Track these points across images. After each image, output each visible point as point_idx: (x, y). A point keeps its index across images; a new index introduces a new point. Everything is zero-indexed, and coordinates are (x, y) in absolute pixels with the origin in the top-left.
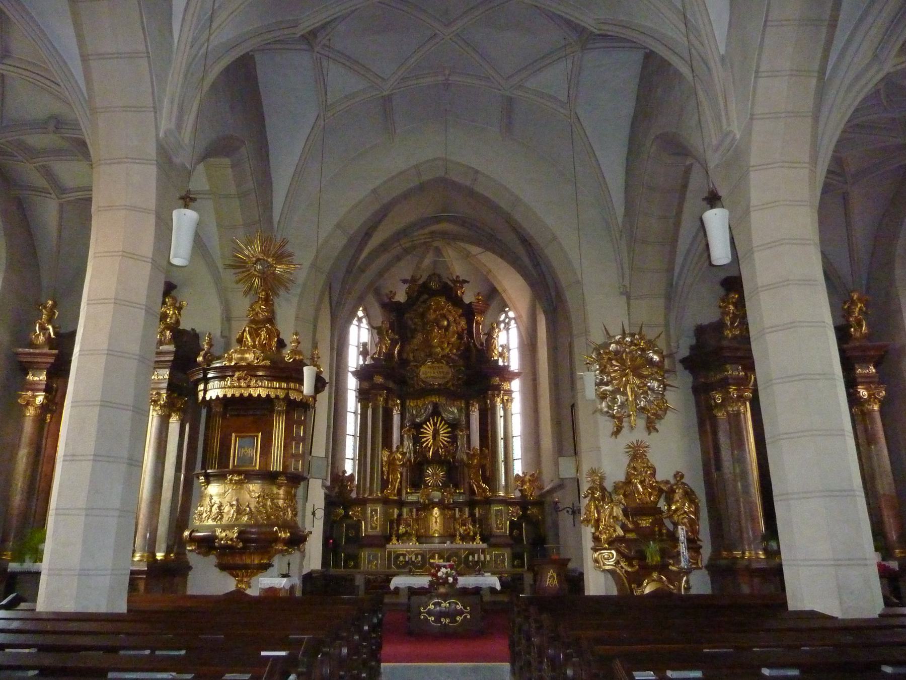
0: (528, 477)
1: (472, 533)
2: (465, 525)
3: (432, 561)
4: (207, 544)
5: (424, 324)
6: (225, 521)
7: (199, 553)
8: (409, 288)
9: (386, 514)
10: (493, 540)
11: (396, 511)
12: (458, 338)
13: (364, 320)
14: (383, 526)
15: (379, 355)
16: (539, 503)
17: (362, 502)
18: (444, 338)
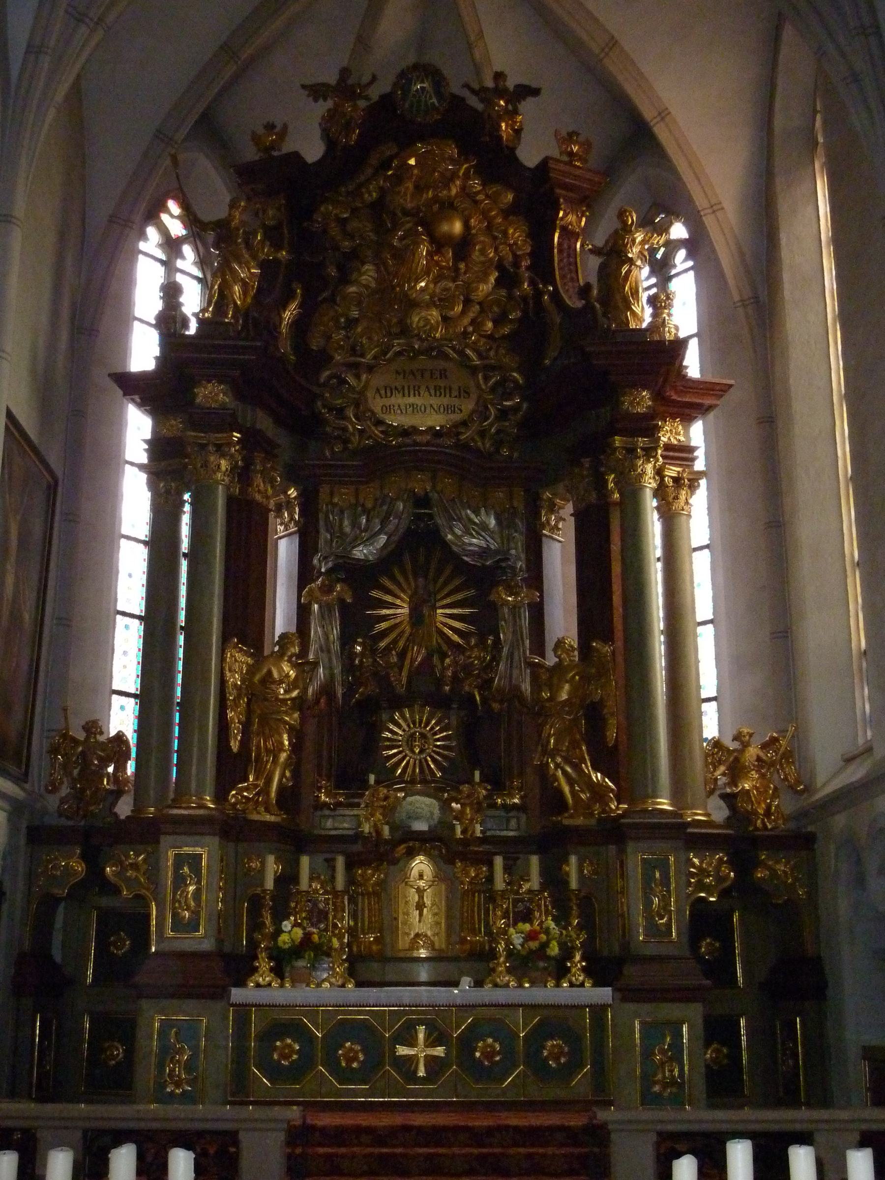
0: (753, 752)
1: (554, 950)
2: (527, 917)
3: (403, 1051)
8: (331, 116)
10: (632, 973)
11: (272, 867)
13: (187, 250)
14: (225, 923)
16: (799, 841)
17: (146, 832)
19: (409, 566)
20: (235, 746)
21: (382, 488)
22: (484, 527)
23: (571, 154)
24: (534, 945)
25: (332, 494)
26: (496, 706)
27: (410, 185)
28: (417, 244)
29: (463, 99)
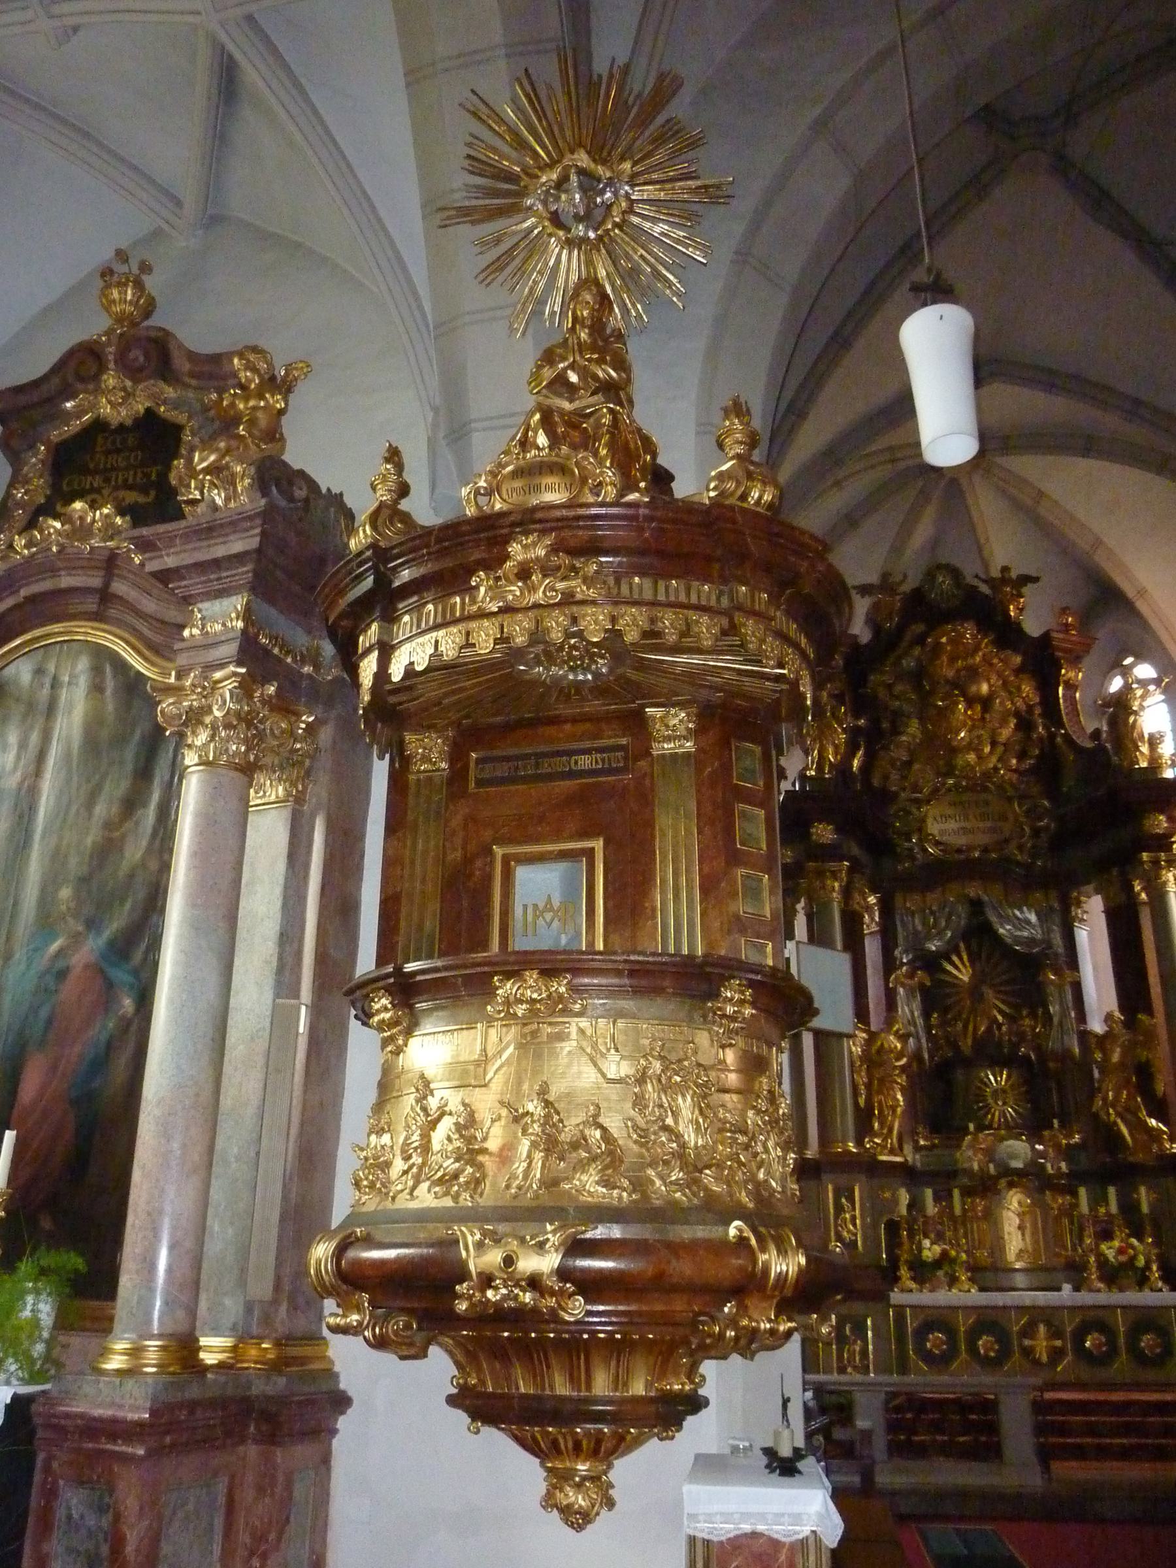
4: (417, 1298)
5: (925, 698)
6: (488, 1197)
7: (380, 1343)
8: (876, 607)
9: (877, 1208)
11: (904, 1197)
12: (1018, 727)
15: (820, 769)
18: (982, 726)
19: (965, 957)
20: (862, 1101)
21: (943, 892)
22: (1028, 922)
23: (1067, 625)
24: (1123, 1258)
25: (905, 902)
26: (1051, 1065)
27: (945, 658)
28: (957, 704)
29: (976, 587)
